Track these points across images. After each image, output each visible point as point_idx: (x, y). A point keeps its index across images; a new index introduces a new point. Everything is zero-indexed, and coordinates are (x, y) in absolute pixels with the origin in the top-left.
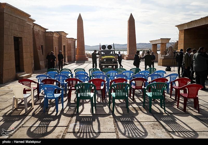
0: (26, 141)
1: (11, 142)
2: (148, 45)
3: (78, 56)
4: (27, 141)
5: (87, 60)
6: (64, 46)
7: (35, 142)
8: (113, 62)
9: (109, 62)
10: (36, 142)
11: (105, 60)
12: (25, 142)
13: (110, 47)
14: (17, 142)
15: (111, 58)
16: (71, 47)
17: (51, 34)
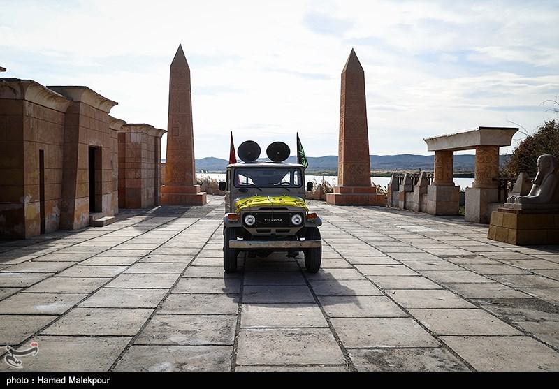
0: (70, 378)
1: (30, 381)
2: (383, 162)
3: (171, 187)
4: (72, 378)
5: (199, 201)
6: (94, 153)
7: (95, 381)
8: (293, 231)
9: (273, 230)
10: (97, 381)
11: (250, 220)
12: (67, 380)
13: (279, 150)
14: (46, 381)
15: (284, 208)
16: (139, 157)
17: (15, 91)
